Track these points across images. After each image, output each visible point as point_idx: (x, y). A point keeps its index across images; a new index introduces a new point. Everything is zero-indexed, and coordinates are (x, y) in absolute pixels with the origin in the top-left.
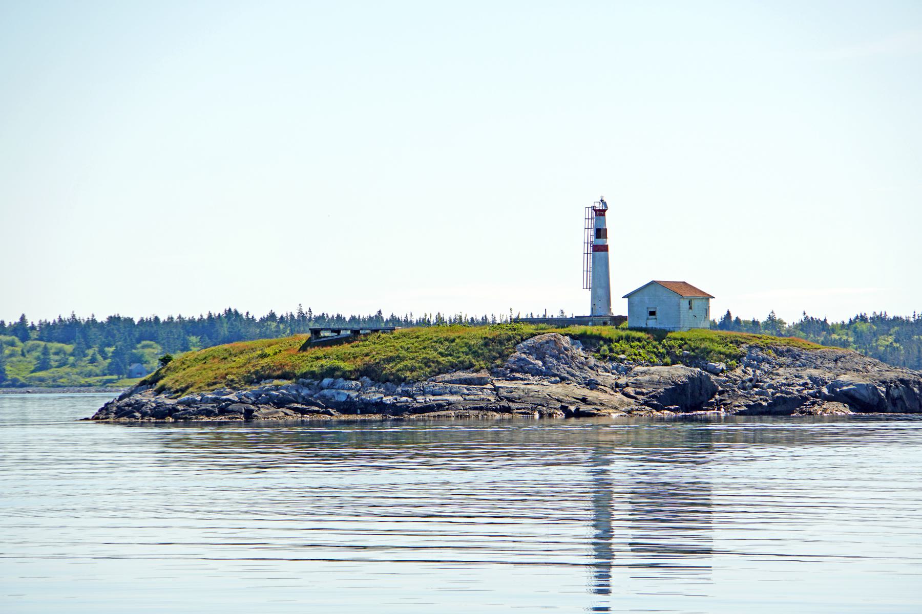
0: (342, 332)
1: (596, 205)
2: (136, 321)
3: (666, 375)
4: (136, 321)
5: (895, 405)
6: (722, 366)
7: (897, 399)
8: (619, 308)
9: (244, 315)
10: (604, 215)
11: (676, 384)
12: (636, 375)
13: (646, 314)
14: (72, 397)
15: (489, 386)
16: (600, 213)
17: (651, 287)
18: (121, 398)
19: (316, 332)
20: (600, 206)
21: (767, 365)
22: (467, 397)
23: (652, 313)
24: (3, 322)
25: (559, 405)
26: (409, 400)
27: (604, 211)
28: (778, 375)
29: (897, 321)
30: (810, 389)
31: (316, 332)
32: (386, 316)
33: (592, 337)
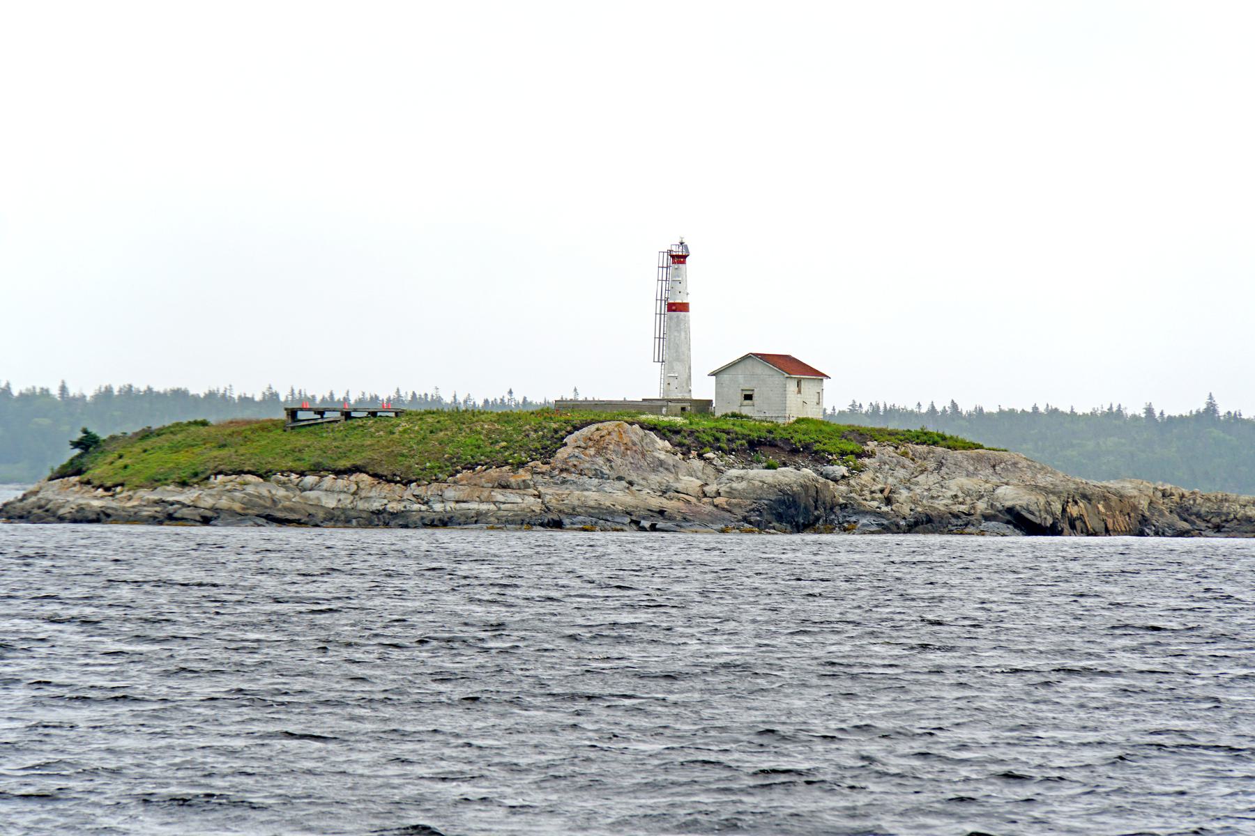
0: (327, 415)
1: (674, 248)
2: (202, 395)
3: (770, 480)
4: (202, 395)
5: (1073, 527)
6: (841, 470)
7: (1078, 518)
8: (703, 389)
9: (55, 391)
10: (684, 262)
11: (785, 493)
12: (730, 480)
13: (740, 397)
14: (277, 601)
15: (532, 491)
16: (679, 259)
17: (749, 362)
18: (25, 497)
19: (293, 413)
20: (678, 251)
21: (902, 471)
22: (502, 506)
23: (748, 397)
24: (6, 391)
25: (627, 520)
26: (424, 508)
27: (685, 257)
28: (917, 484)
29: (1182, 418)
30: (961, 503)
31: (293, 413)
32: (368, 396)
33: (693, 431)
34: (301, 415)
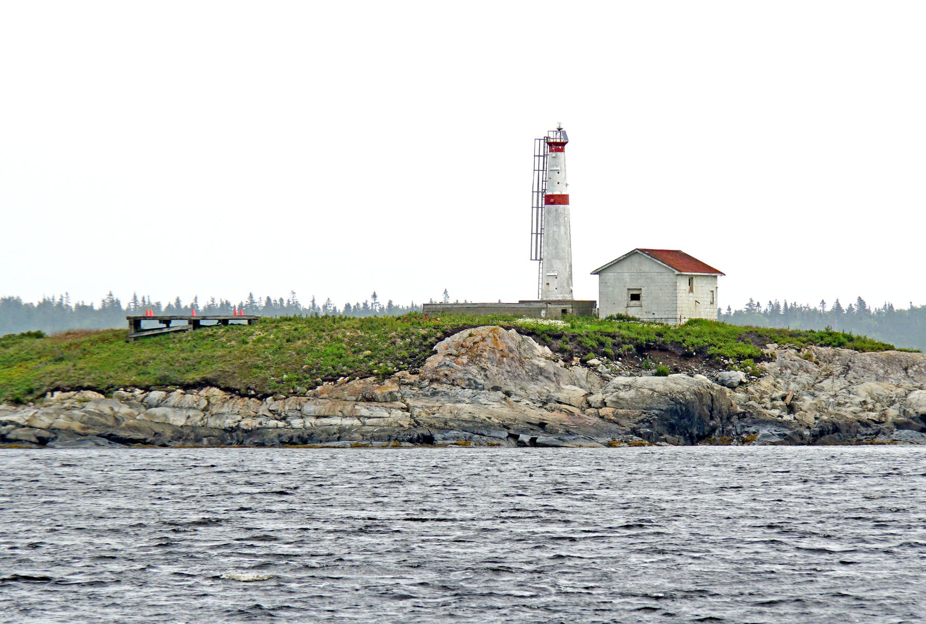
1: (551, 135)
8: (586, 289)
12: (617, 388)
13: (626, 297)
15: (399, 404)
19: (136, 322)
20: (556, 138)
21: (806, 375)
22: (368, 421)
23: (636, 297)
25: (505, 434)
26: (281, 424)
27: (563, 144)
28: (822, 389)
31: (136, 322)
34: (145, 324)
